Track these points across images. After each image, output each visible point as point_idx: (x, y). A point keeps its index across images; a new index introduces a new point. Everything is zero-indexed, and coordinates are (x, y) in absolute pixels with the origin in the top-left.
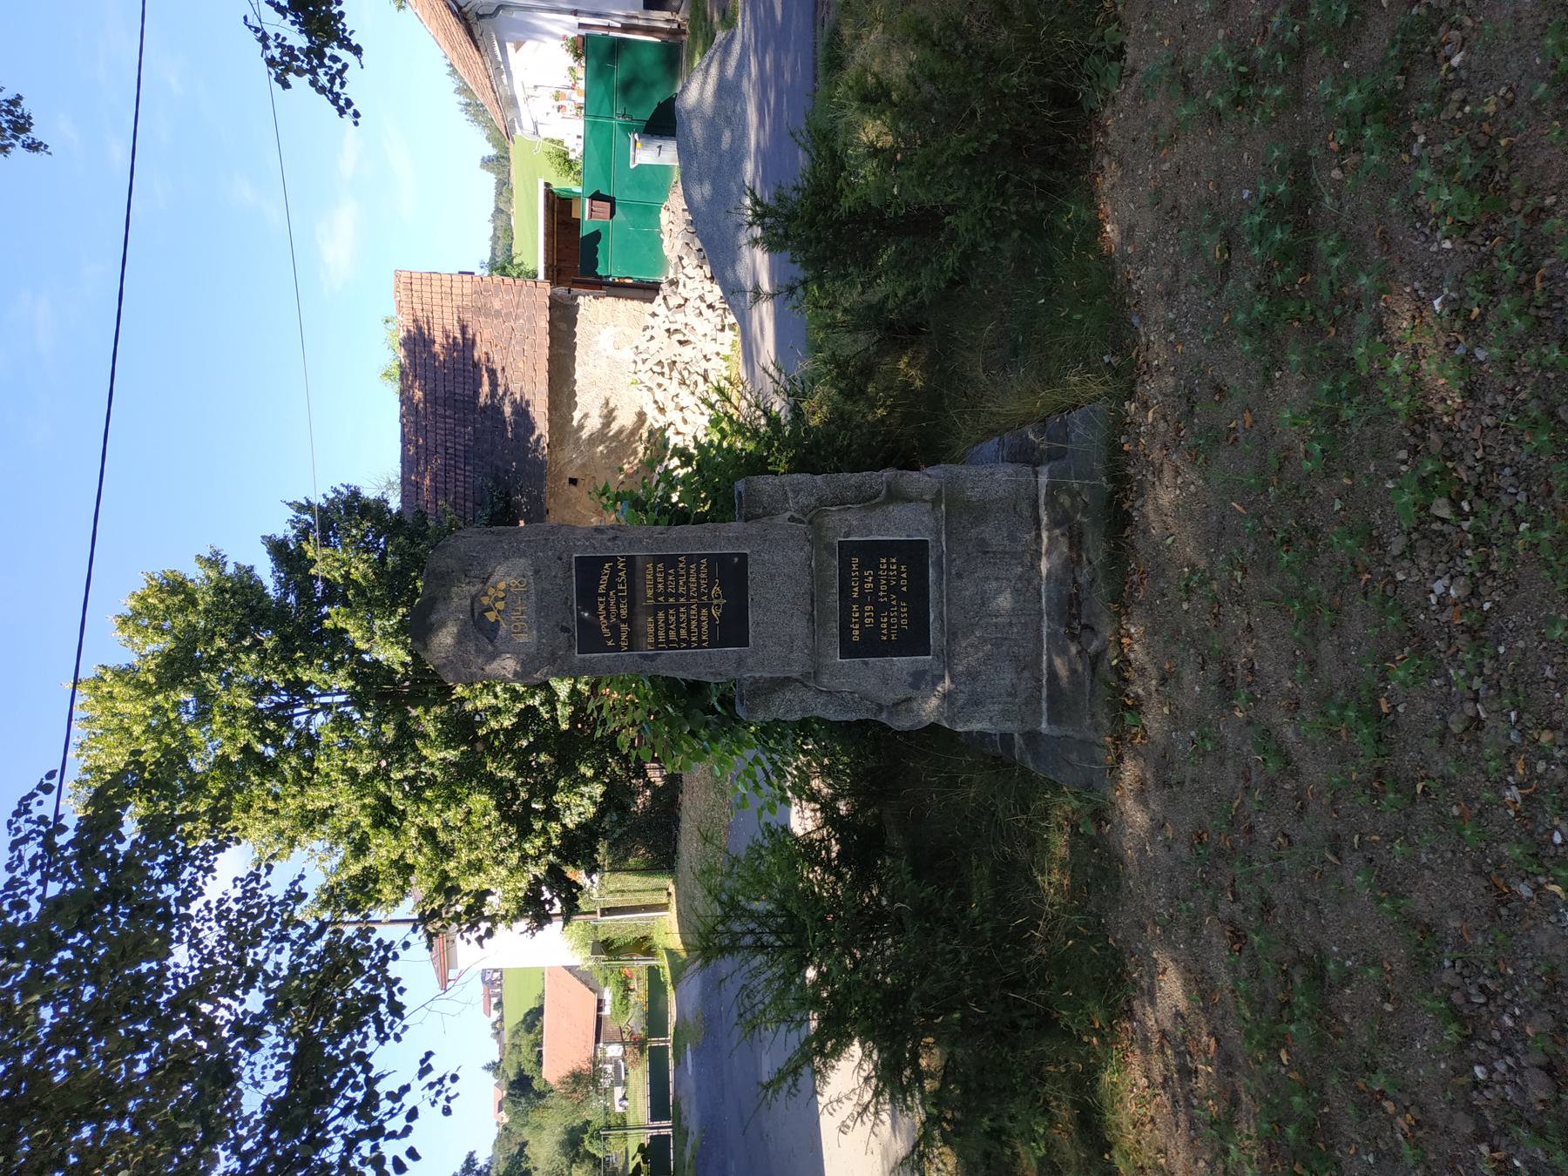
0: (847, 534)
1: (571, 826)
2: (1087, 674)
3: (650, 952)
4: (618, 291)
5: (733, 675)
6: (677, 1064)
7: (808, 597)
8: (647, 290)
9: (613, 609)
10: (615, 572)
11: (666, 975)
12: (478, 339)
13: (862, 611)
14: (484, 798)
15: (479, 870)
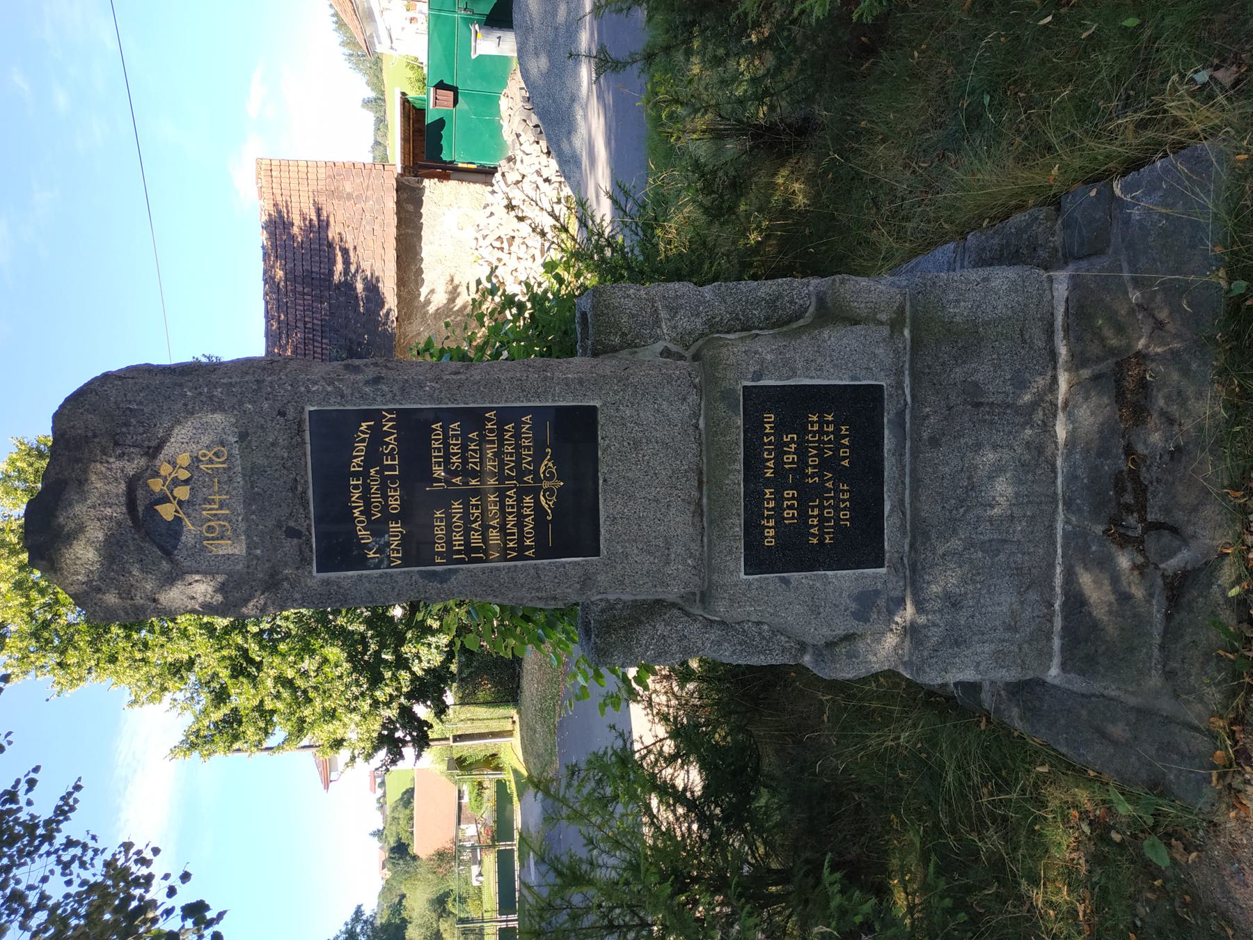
0: (758, 376)
1: (420, 673)
2: (1156, 611)
3: (498, 768)
4: (461, 175)
5: (574, 598)
6: (522, 866)
7: (693, 477)
8: (485, 174)
9: (376, 498)
10: (377, 436)
11: (512, 787)
12: (332, 220)
13: (779, 499)
14: (336, 650)
15: (333, 717)
